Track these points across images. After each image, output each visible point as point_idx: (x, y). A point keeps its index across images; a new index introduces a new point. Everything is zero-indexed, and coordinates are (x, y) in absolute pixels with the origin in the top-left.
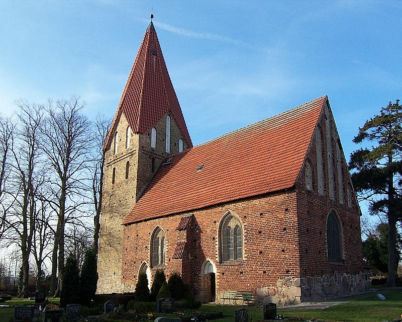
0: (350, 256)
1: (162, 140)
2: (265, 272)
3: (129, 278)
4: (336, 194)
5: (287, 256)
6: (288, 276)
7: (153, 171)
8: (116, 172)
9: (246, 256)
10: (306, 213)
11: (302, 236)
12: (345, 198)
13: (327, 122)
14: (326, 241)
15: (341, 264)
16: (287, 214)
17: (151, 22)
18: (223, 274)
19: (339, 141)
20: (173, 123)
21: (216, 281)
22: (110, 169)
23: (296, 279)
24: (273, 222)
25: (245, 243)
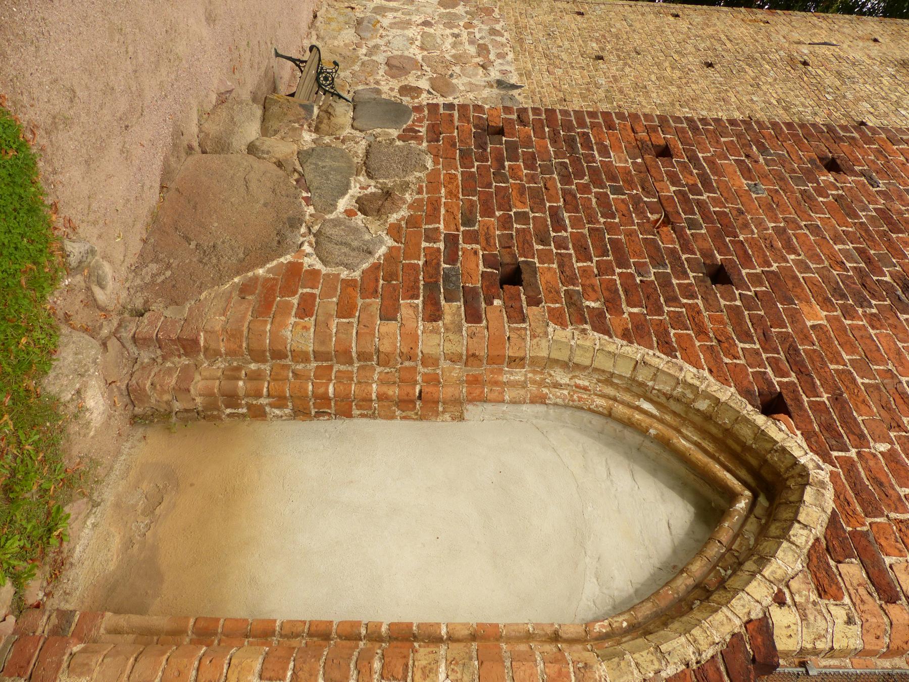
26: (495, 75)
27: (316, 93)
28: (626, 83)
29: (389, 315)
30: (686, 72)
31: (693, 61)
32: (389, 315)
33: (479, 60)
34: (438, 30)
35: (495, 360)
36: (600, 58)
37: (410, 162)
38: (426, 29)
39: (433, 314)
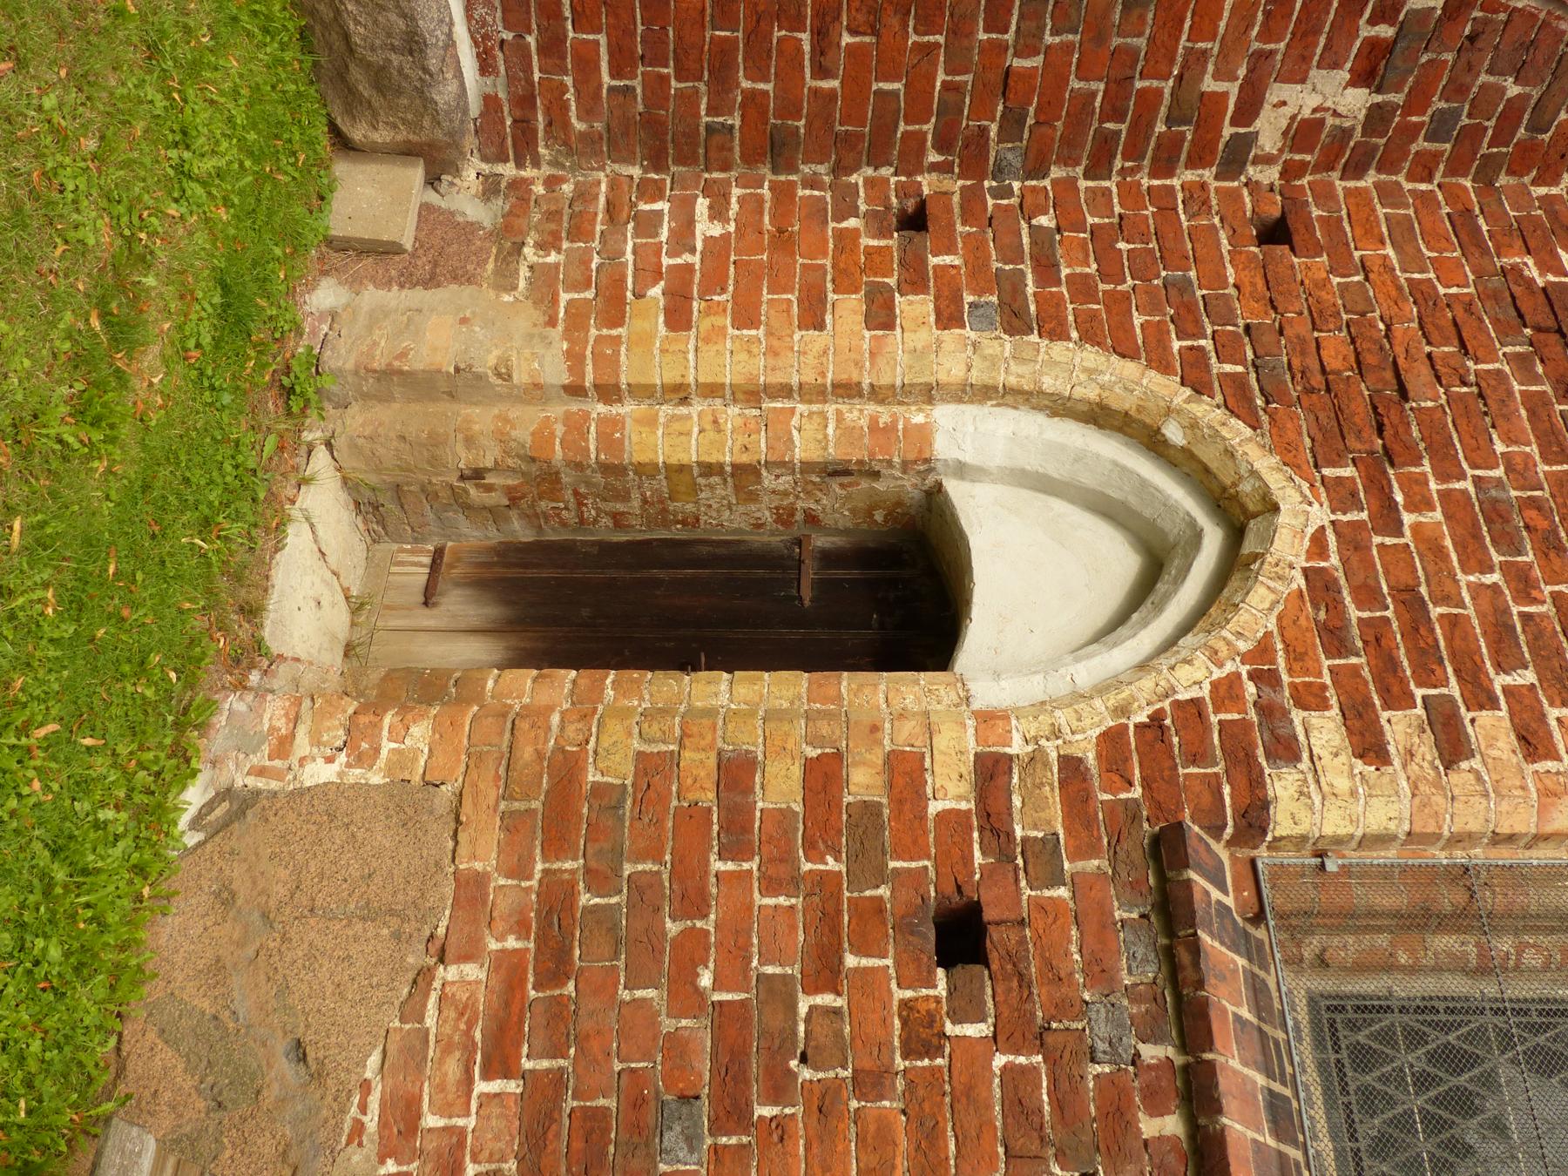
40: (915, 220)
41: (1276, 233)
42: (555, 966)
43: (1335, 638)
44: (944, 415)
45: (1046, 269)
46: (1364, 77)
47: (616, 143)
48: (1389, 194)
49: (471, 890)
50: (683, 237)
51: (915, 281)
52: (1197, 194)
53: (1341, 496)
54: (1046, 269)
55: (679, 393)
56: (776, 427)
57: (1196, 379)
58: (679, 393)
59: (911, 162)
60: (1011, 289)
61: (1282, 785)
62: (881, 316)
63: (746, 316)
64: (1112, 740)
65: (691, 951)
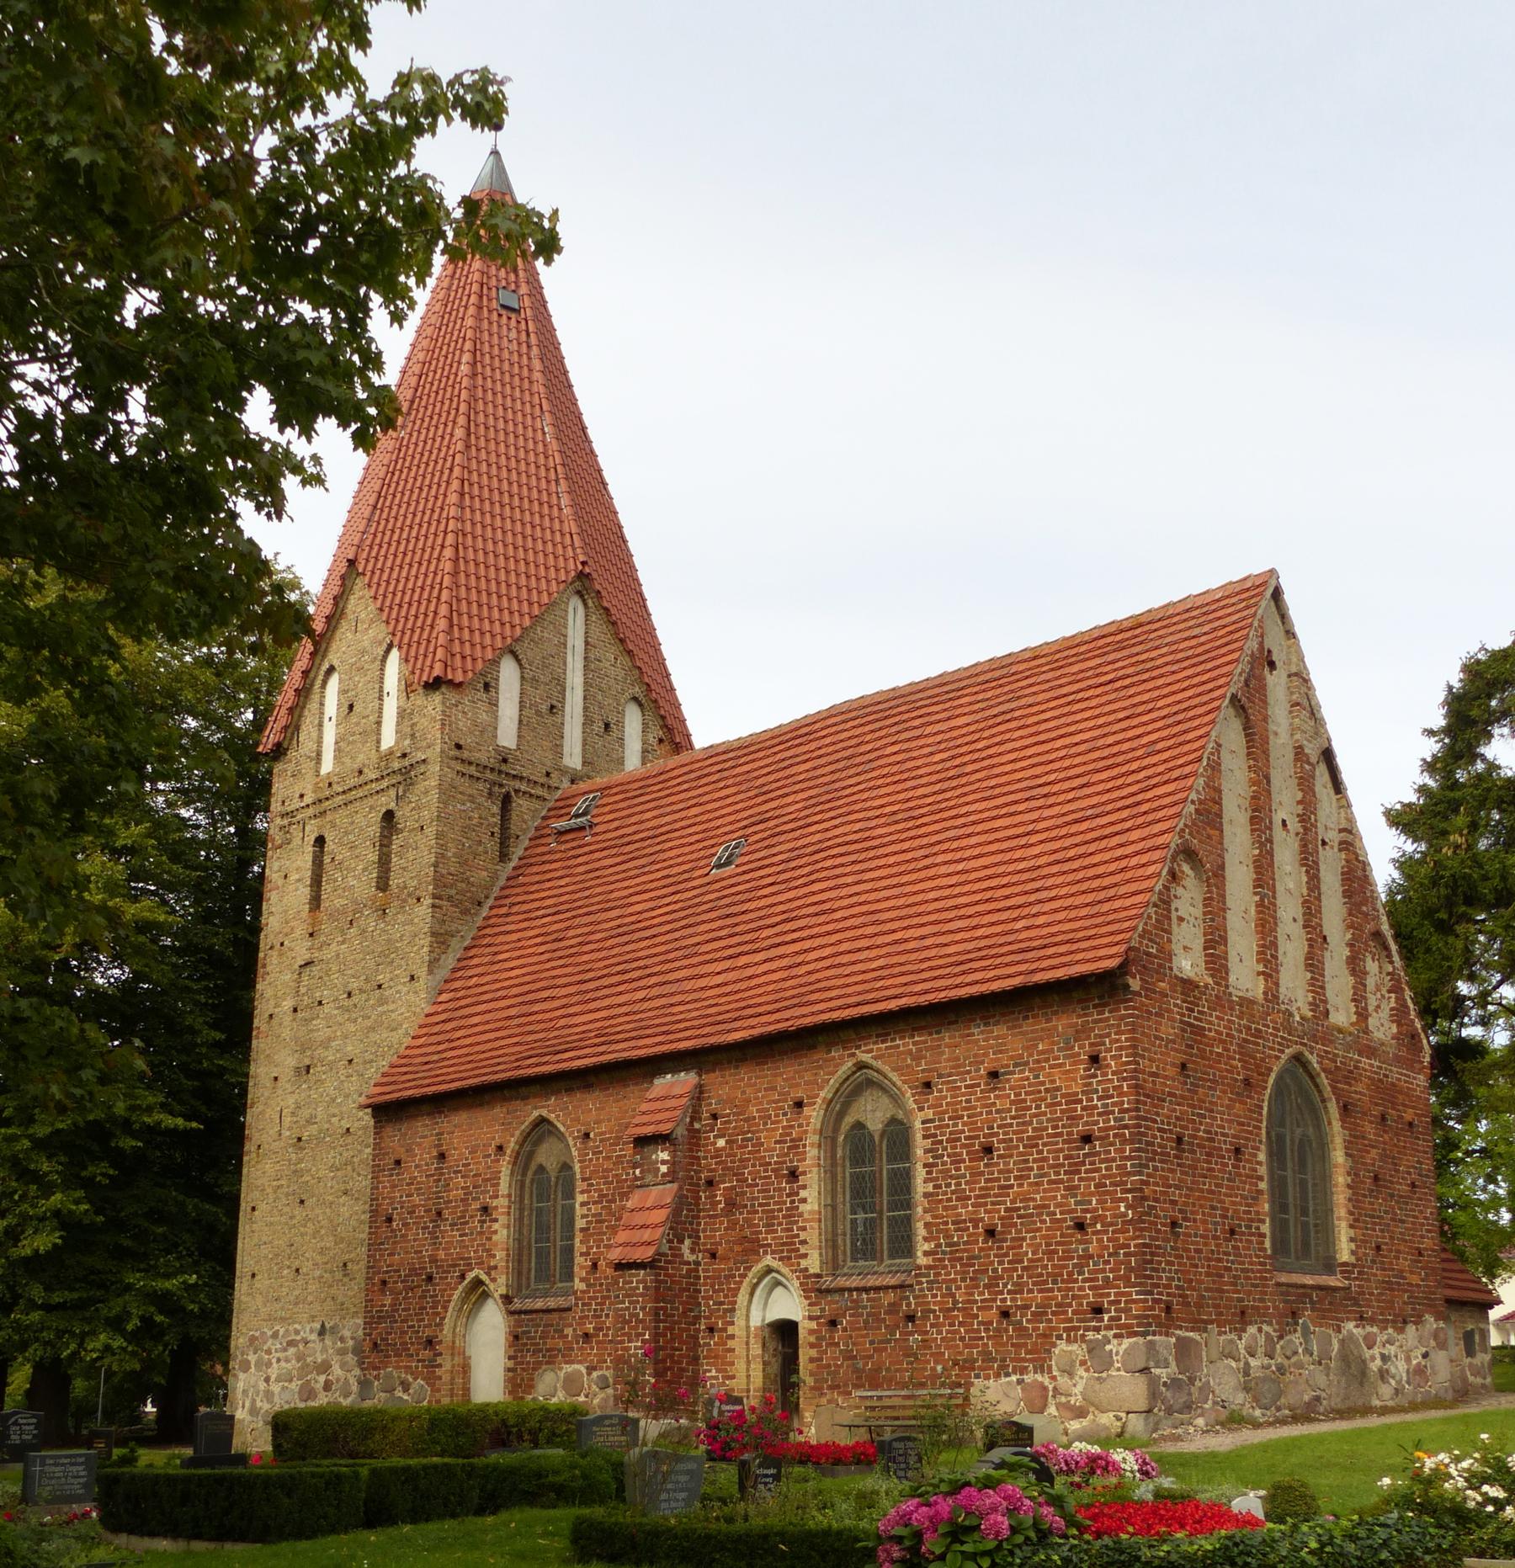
0: (1378, 1248)
1: (544, 708)
2: (1005, 1314)
3: (402, 1351)
4: (1317, 986)
5: (1093, 1248)
6: (1097, 1330)
7: (504, 856)
8: (327, 859)
9: (926, 1247)
10: (1171, 1071)
11: (1155, 1169)
12: (1359, 998)
13: (1276, 682)
14: (1263, 1185)
15: (1333, 1281)
16: (1095, 1076)
17: (495, 153)
18: (833, 1323)
19: (1328, 755)
20: (600, 630)
21: (805, 1354)
22: (297, 841)
23: (1127, 1342)
24: (1038, 1107)
25: (926, 1195)
26: (314, 1337)
27: (642, 1142)
28: (319, 1259)
29: (440, 1378)
30: (307, 1219)
31: (298, 1211)
32: (440, 1378)
33: (301, 1346)
34: (273, 1372)
35: (453, 1348)
36: (297, 1270)
37: (389, 1376)
38: (273, 1379)
39: (440, 1366)
40: (711, 1330)
41: (713, 1256)
42: (838, 1387)
43: (789, 1258)
44: (752, 1324)
45: (722, 1303)
46: (681, 1241)
47: (695, 1392)
48: (704, 1231)
49: (829, 1402)
50: (716, 1378)
51: (725, 1330)
52: (704, 1271)
53: (766, 1253)
54: (722, 1303)
55: (748, 1376)
56: (755, 1357)
57: (744, 1276)
58: (748, 1376)
59: (698, 1330)
60: (726, 1311)
61: (812, 1271)
62: (732, 1337)
63: (733, 1364)
64: (806, 1298)
65: (836, 1366)
